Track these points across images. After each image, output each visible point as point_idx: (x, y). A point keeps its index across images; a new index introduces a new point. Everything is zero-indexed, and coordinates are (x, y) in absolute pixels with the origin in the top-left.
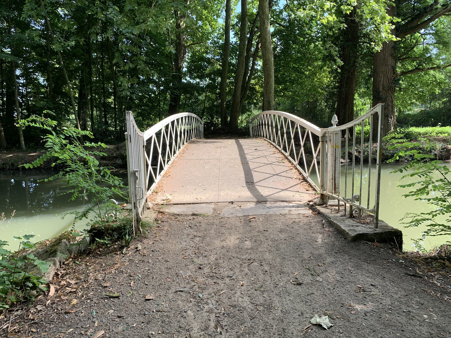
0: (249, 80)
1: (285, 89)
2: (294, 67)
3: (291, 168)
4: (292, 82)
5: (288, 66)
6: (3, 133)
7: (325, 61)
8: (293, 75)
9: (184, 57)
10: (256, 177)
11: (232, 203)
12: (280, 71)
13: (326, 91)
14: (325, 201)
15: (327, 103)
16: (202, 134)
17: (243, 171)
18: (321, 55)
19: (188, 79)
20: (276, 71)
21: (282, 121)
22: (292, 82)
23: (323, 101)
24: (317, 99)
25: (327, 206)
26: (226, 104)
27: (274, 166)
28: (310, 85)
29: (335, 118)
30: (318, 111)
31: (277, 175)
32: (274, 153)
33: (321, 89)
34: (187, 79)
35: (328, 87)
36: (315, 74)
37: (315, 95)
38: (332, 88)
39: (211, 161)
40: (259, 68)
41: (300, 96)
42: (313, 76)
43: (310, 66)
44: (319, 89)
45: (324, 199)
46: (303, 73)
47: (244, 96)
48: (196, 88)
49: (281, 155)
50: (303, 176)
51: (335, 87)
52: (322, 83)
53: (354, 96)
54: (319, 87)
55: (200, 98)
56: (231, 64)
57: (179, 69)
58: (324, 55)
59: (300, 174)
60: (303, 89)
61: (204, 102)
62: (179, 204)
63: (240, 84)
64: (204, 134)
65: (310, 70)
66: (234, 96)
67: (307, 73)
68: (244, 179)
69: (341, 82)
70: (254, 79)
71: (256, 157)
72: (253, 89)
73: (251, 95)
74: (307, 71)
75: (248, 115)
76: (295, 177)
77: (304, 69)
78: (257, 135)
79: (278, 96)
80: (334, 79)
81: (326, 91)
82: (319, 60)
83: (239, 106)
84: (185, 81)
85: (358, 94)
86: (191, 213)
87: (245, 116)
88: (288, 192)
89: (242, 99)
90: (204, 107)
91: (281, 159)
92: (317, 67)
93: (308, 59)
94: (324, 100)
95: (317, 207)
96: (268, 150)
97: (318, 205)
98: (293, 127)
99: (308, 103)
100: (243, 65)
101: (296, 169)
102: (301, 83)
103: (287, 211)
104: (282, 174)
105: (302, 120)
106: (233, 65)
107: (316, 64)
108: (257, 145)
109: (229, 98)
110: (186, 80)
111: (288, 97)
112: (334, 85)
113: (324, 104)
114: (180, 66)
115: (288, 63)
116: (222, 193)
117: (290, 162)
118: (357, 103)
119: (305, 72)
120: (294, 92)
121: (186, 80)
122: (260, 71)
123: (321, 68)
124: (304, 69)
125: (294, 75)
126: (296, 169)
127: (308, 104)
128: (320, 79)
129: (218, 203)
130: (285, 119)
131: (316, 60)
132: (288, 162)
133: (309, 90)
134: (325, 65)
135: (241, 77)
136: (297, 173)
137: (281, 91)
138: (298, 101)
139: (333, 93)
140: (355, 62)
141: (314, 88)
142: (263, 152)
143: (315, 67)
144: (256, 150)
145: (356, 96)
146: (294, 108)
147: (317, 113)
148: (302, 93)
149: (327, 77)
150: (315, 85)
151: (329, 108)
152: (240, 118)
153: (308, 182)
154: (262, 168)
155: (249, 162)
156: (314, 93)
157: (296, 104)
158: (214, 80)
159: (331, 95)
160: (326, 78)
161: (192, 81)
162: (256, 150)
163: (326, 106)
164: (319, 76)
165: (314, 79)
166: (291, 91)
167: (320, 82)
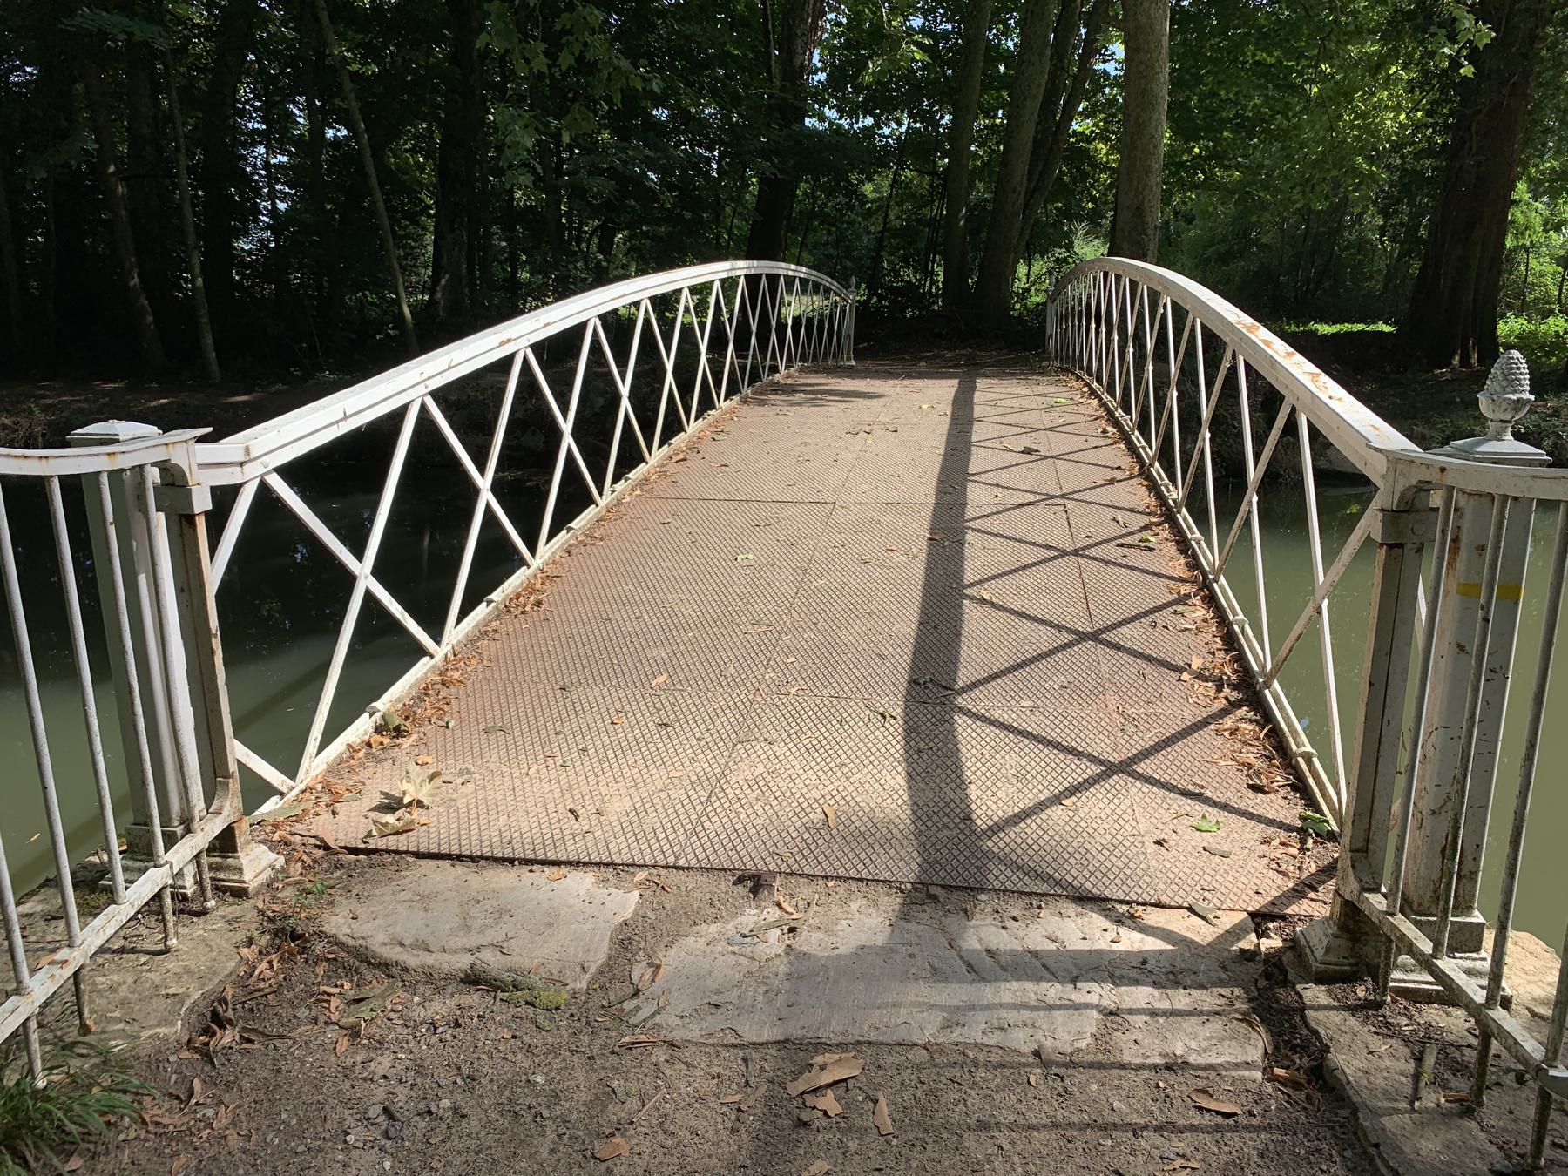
0: (1068, 118)
1: (1217, 156)
2: (1257, 63)
3: (1186, 589)
4: (1245, 128)
5: (1235, 60)
6: (150, 319)
7: (1399, 36)
8: (1252, 98)
9: (815, 28)
10: (983, 639)
11: (756, 883)
12: (1198, 80)
13: (1388, 167)
14: (1369, 951)
15: (1386, 216)
16: (848, 343)
17: (917, 595)
18: (1380, 14)
19: (832, 114)
20: (1177, 82)
21: (1164, 316)
22: (1245, 128)
23: (1371, 210)
24: (1346, 198)
25: (1378, 1005)
26: (968, 218)
27: (1091, 568)
28: (1322, 141)
29: (1510, 382)
30: (1347, 248)
31: (1095, 636)
32: (1112, 482)
33: (1370, 160)
34: (824, 119)
35: (1397, 148)
36: (1346, 95)
37: (1337, 185)
38: (1418, 156)
39: (790, 511)
40: (1111, 68)
41: (1275, 187)
42: (1338, 105)
43: (1329, 59)
44: (1360, 159)
45: (1359, 951)
46: (1299, 91)
47: (1043, 190)
48: (859, 154)
49: (1143, 492)
50: (1241, 659)
51: (1430, 152)
52: (1372, 130)
53: (1513, 187)
54: (1360, 151)
55: (868, 188)
56: (995, 54)
57: (795, 72)
58: (1396, 11)
59: (1230, 641)
60: (1289, 158)
61: (883, 205)
62: (448, 857)
63: (1028, 132)
64: (858, 338)
65: (1327, 78)
66: (1001, 187)
67: (1315, 90)
68: (904, 658)
69: (1460, 130)
70: (1086, 115)
71: (1013, 499)
72: (1080, 156)
73: (1074, 180)
74: (1312, 82)
75: (1057, 261)
76: (1196, 664)
77: (1300, 74)
78: (1068, 363)
79: (1182, 184)
80: (1429, 114)
81: (1388, 167)
82: (1372, 32)
83: (1018, 225)
84: (820, 127)
85: (1530, 180)
86: (462, 962)
87: (1039, 266)
88: (1137, 789)
89: (1031, 194)
90: (885, 229)
91: (1139, 521)
92: (1357, 64)
93: (1320, 30)
94: (1375, 204)
95: (1314, 994)
96: (1089, 456)
97: (1320, 979)
98: (1212, 365)
99: (1306, 214)
100: (1042, 55)
101: (1211, 600)
102: (1286, 132)
103: (1091, 1022)
104: (1126, 635)
105: (1262, 335)
106: (1006, 57)
107: (1354, 51)
108: (1046, 420)
109: (980, 191)
110: (822, 119)
111: (1227, 191)
112: (1429, 139)
113: (1373, 219)
114: (798, 62)
115: (1238, 45)
116: (747, 769)
117: (1184, 545)
118: (1520, 218)
119: (1307, 87)
120: (1251, 171)
121: (822, 119)
122: (1115, 83)
123: (1377, 66)
124: (1300, 74)
125: (1257, 100)
126: (1211, 600)
127: (1307, 221)
128: (1364, 115)
129: (675, 877)
130: (1180, 313)
131: (1360, 32)
132: (1171, 548)
133: (1316, 164)
134: (1393, 56)
135: (1033, 107)
136: (1211, 636)
137: (1198, 162)
138: (1263, 206)
139: (1418, 174)
140: (1533, 38)
141: (1338, 153)
142: (1062, 466)
143: (1347, 66)
144: (1027, 451)
145: (1521, 189)
146: (1246, 234)
147: (1339, 257)
148: (1284, 175)
149: (1397, 109)
150: (1344, 141)
151: (1393, 240)
152: (1022, 269)
153: (1265, 716)
154: (1024, 578)
155: (970, 537)
156: (1334, 173)
157: (1254, 219)
158: (929, 119)
159: (1409, 183)
160: (1394, 112)
161: (845, 123)
162: (1027, 451)
163: (1382, 230)
164: (1364, 102)
165: (1340, 117)
166: (1238, 166)
167: (1366, 129)
